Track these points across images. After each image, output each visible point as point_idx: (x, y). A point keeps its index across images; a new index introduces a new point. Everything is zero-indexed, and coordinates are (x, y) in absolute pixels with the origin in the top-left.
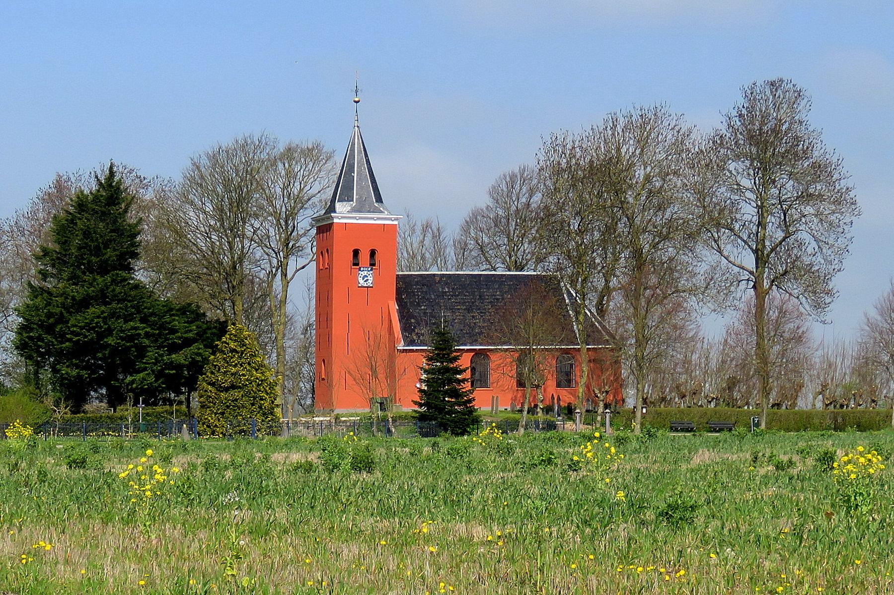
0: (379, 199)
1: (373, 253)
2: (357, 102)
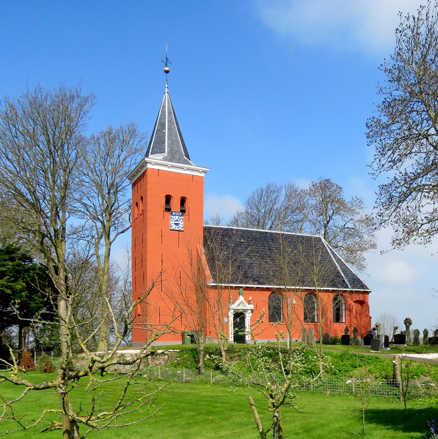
0: (187, 156)
1: (183, 201)
2: (167, 72)
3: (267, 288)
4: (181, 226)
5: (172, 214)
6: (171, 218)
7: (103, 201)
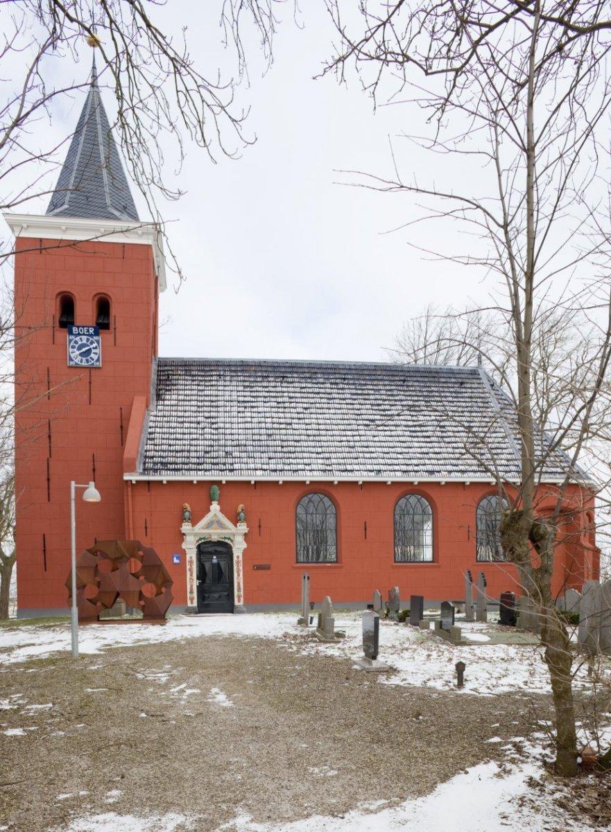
1: (103, 307)
3: (169, 482)
4: (95, 357)
5: (71, 333)
6: (70, 341)
7: (455, 421)
